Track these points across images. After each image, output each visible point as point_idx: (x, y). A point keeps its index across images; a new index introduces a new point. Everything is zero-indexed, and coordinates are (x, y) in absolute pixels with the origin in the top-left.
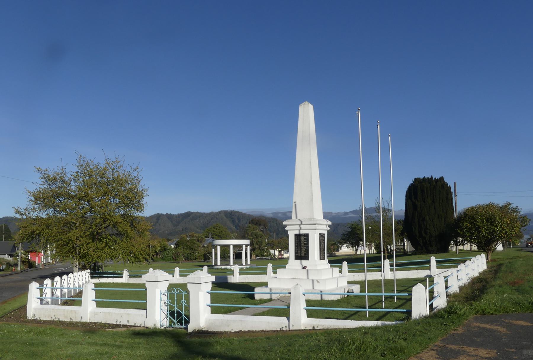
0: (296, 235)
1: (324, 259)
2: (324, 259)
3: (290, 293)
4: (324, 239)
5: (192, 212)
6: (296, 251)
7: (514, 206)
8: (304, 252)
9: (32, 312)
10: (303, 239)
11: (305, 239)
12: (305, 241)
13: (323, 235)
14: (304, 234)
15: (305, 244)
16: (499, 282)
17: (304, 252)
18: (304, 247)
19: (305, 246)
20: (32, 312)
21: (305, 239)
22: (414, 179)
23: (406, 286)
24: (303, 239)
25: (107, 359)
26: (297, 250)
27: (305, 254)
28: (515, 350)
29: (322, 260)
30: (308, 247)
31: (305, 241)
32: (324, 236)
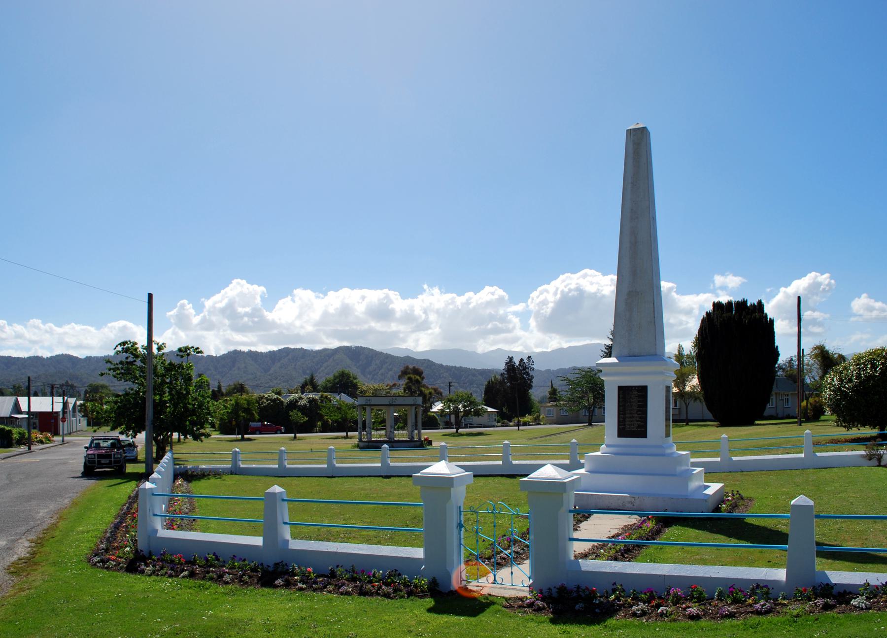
0: (621, 388)
10: (636, 397)
15: (639, 406)
19: (638, 411)
27: (639, 426)
30: (645, 413)
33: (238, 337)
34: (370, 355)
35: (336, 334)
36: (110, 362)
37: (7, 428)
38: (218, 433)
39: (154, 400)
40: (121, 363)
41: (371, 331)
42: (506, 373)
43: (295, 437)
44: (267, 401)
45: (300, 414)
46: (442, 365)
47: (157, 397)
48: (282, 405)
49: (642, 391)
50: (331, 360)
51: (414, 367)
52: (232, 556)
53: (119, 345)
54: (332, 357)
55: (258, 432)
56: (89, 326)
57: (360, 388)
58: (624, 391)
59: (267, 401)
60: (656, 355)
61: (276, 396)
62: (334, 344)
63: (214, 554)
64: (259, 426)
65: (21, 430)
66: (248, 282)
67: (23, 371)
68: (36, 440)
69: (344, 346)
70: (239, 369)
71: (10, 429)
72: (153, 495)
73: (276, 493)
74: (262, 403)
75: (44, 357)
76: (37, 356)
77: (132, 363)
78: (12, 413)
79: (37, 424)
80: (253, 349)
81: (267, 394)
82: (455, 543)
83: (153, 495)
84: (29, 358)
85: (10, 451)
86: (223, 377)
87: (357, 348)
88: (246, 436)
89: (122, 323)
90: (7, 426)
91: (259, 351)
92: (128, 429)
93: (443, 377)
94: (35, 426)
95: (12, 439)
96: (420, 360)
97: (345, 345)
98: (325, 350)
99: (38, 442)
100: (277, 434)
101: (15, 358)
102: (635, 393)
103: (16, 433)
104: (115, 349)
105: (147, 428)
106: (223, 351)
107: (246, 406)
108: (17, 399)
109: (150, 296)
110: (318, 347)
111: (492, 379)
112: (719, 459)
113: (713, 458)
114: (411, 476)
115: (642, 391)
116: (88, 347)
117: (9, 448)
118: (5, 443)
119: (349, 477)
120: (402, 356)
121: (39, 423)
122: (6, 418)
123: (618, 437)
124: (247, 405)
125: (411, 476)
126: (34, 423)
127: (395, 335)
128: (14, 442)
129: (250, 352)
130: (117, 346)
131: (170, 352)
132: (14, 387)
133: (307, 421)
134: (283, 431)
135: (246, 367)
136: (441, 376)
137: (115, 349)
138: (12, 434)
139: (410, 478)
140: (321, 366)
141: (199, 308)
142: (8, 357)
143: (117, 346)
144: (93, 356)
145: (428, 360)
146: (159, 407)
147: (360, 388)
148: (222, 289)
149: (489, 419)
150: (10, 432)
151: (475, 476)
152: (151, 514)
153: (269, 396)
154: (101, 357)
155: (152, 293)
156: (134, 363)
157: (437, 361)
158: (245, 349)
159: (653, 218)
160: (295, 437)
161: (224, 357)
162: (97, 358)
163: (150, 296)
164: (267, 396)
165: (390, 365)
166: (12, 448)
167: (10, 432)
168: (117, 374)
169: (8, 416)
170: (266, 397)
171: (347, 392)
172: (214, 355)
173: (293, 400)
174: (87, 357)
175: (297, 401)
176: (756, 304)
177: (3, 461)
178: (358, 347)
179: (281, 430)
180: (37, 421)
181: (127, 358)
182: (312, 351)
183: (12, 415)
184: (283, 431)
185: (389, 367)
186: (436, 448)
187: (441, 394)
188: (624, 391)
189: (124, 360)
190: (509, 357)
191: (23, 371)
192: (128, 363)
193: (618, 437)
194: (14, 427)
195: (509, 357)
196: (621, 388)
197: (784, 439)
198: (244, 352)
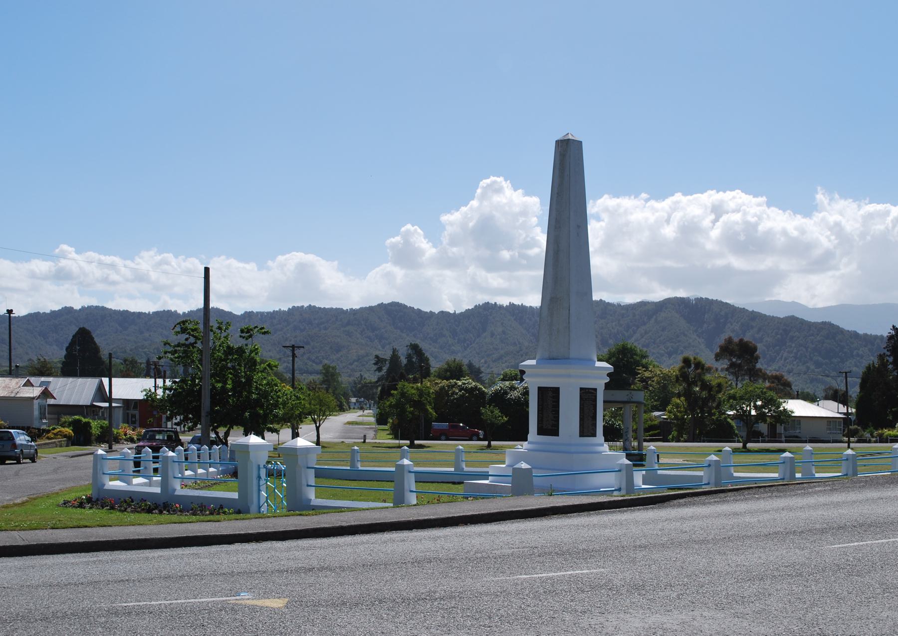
0: (540, 389)
33: (495, 280)
34: (723, 313)
35: (665, 277)
36: (169, 344)
37: (84, 420)
38: (391, 437)
39: (214, 387)
40: (179, 345)
41: (728, 272)
42: (889, 353)
43: (489, 446)
44: (460, 391)
45: (497, 412)
46: (855, 332)
47: (220, 385)
48: (484, 397)
49: (556, 391)
50: (652, 321)
51: (741, 340)
52: (140, 499)
53: (178, 324)
54: (655, 317)
55: (443, 437)
57: (640, 374)
58: (542, 391)
59: (460, 391)
60: (569, 358)
61: (474, 384)
62: (659, 294)
63: (130, 498)
64: (445, 428)
65: (104, 423)
67: (147, 335)
68: (124, 437)
69: (676, 298)
70: (492, 335)
71: (87, 420)
72: (103, 459)
73: (168, 456)
74: (454, 393)
75: (178, 312)
76: (168, 311)
77: (192, 345)
78: (93, 400)
79: (137, 417)
80: (517, 301)
81: (460, 380)
82: (255, 488)
83: (103, 459)
84: (157, 314)
85: (85, 449)
86: (465, 349)
87: (699, 300)
88: (416, 442)
89: (297, 257)
90: (85, 417)
91: (528, 305)
92: (186, 419)
93: (858, 355)
94: (134, 419)
95: (91, 434)
96: (814, 323)
97: (678, 296)
98: (643, 304)
99: (126, 440)
100: (440, 440)
101: (134, 313)
103: (95, 426)
104: (174, 328)
105: (203, 419)
106: (467, 305)
107: (416, 398)
108: (101, 381)
109: (207, 270)
110: (630, 299)
111: (873, 363)
114: (463, 483)
115: (556, 391)
116: (242, 296)
117: (86, 446)
118: (82, 439)
119: (424, 482)
120: (782, 317)
121: (140, 416)
122: (87, 406)
123: (538, 434)
124: (419, 396)
125: (463, 483)
126: (134, 416)
127: (775, 277)
128: (93, 438)
129: (512, 306)
130: (175, 326)
131: (379, 305)
132: (125, 361)
133: (507, 421)
134: (482, 437)
135: (504, 332)
136: (855, 353)
137: (174, 328)
138: (91, 427)
139: (462, 485)
140: (635, 332)
141: (433, 232)
142: (124, 311)
143: (175, 326)
144: (255, 311)
145: (830, 325)
146: (218, 397)
147: (640, 374)
149: (830, 429)
150: (88, 424)
152: (101, 472)
153: (465, 384)
154: (268, 313)
155: (208, 266)
156: (195, 345)
157: (847, 325)
158: (504, 301)
159: (579, 227)
160: (489, 446)
161: (468, 314)
162: (262, 314)
163: (207, 270)
164: (460, 384)
165: (760, 330)
166: (91, 446)
167: (88, 424)
168: (176, 358)
169: (89, 404)
170: (459, 386)
172: (452, 312)
173: (500, 391)
174: (246, 312)
175: (506, 393)
178: (702, 298)
179: (477, 434)
180: (137, 413)
181: (187, 339)
182: (619, 305)
183: (94, 403)
184: (482, 437)
185: (756, 335)
187: (788, 384)
189: (183, 341)
190: (893, 326)
191: (147, 335)
192: (187, 346)
193: (538, 434)
194: (95, 419)
195: (893, 326)
196: (540, 389)
198: (501, 307)
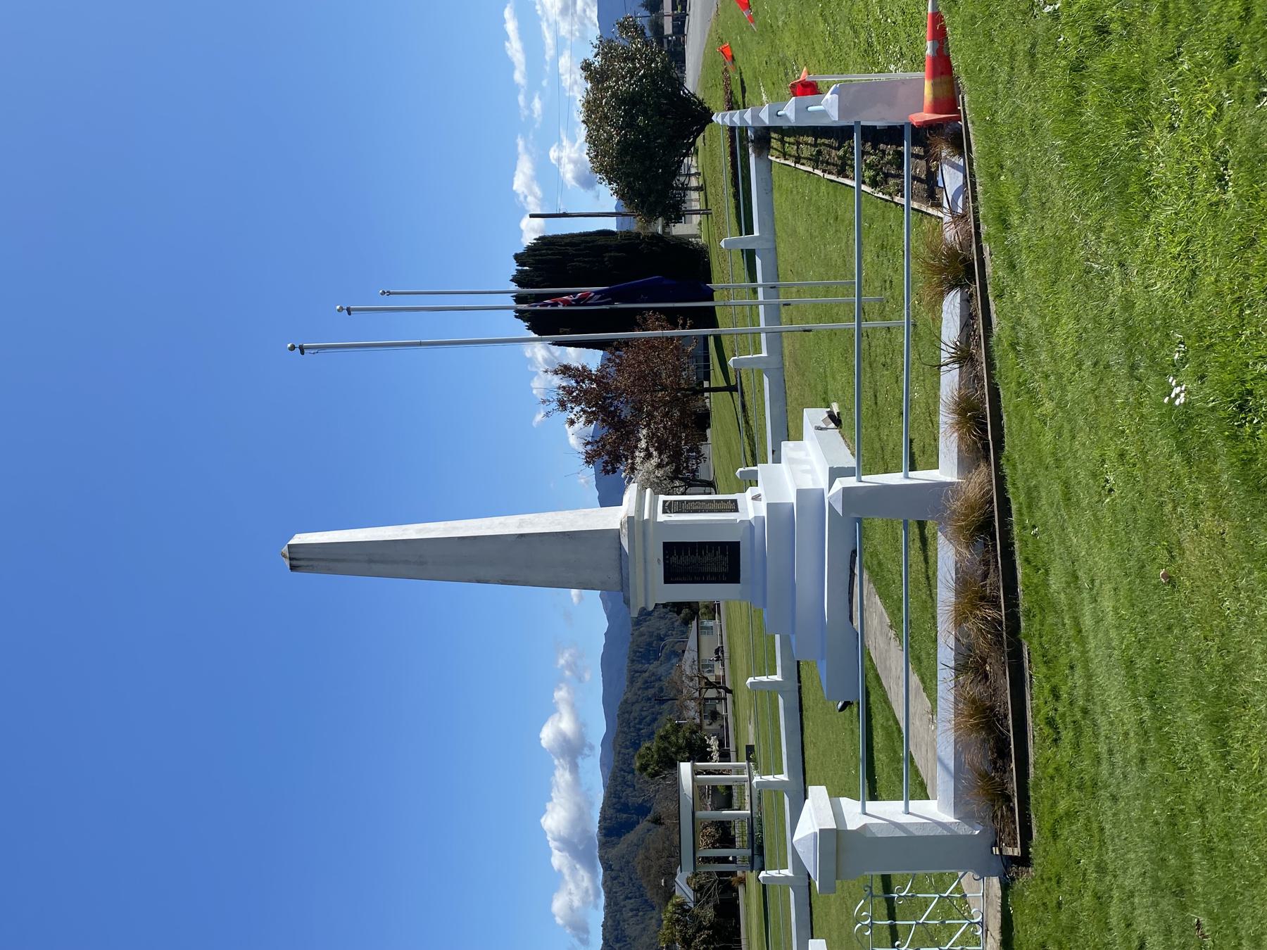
0: (668, 580)
1: (735, 501)
2: (735, 501)
3: (742, 250)
4: (679, 501)
5: (602, 942)
6: (643, 499)
7: (590, 54)
8: (715, 555)
9: (774, 873)
10: (679, 558)
11: (679, 554)
12: (686, 554)
13: (667, 504)
14: (665, 555)
15: (693, 553)
16: (1017, 904)
17: (715, 555)
18: (701, 556)
19: (700, 554)
20: (774, 873)
21: (679, 554)
22: (820, 830)
23: (744, 97)
24: (679, 558)
25: (1087, 949)
26: (711, 576)
27: (723, 553)
28: (1136, 674)
29: (739, 507)
30: (702, 545)
31: (686, 554)
32: (671, 501)
56: (605, 892)
58: (671, 576)
66: (546, 835)
102: (674, 559)
112: (777, 637)
113: (791, 906)
148: (520, 239)
151: (812, 938)
171: (667, 557)
176: (527, 324)
177: (715, 2)
186: (757, 739)
188: (671, 576)
196: (668, 580)
197: (759, 715)
